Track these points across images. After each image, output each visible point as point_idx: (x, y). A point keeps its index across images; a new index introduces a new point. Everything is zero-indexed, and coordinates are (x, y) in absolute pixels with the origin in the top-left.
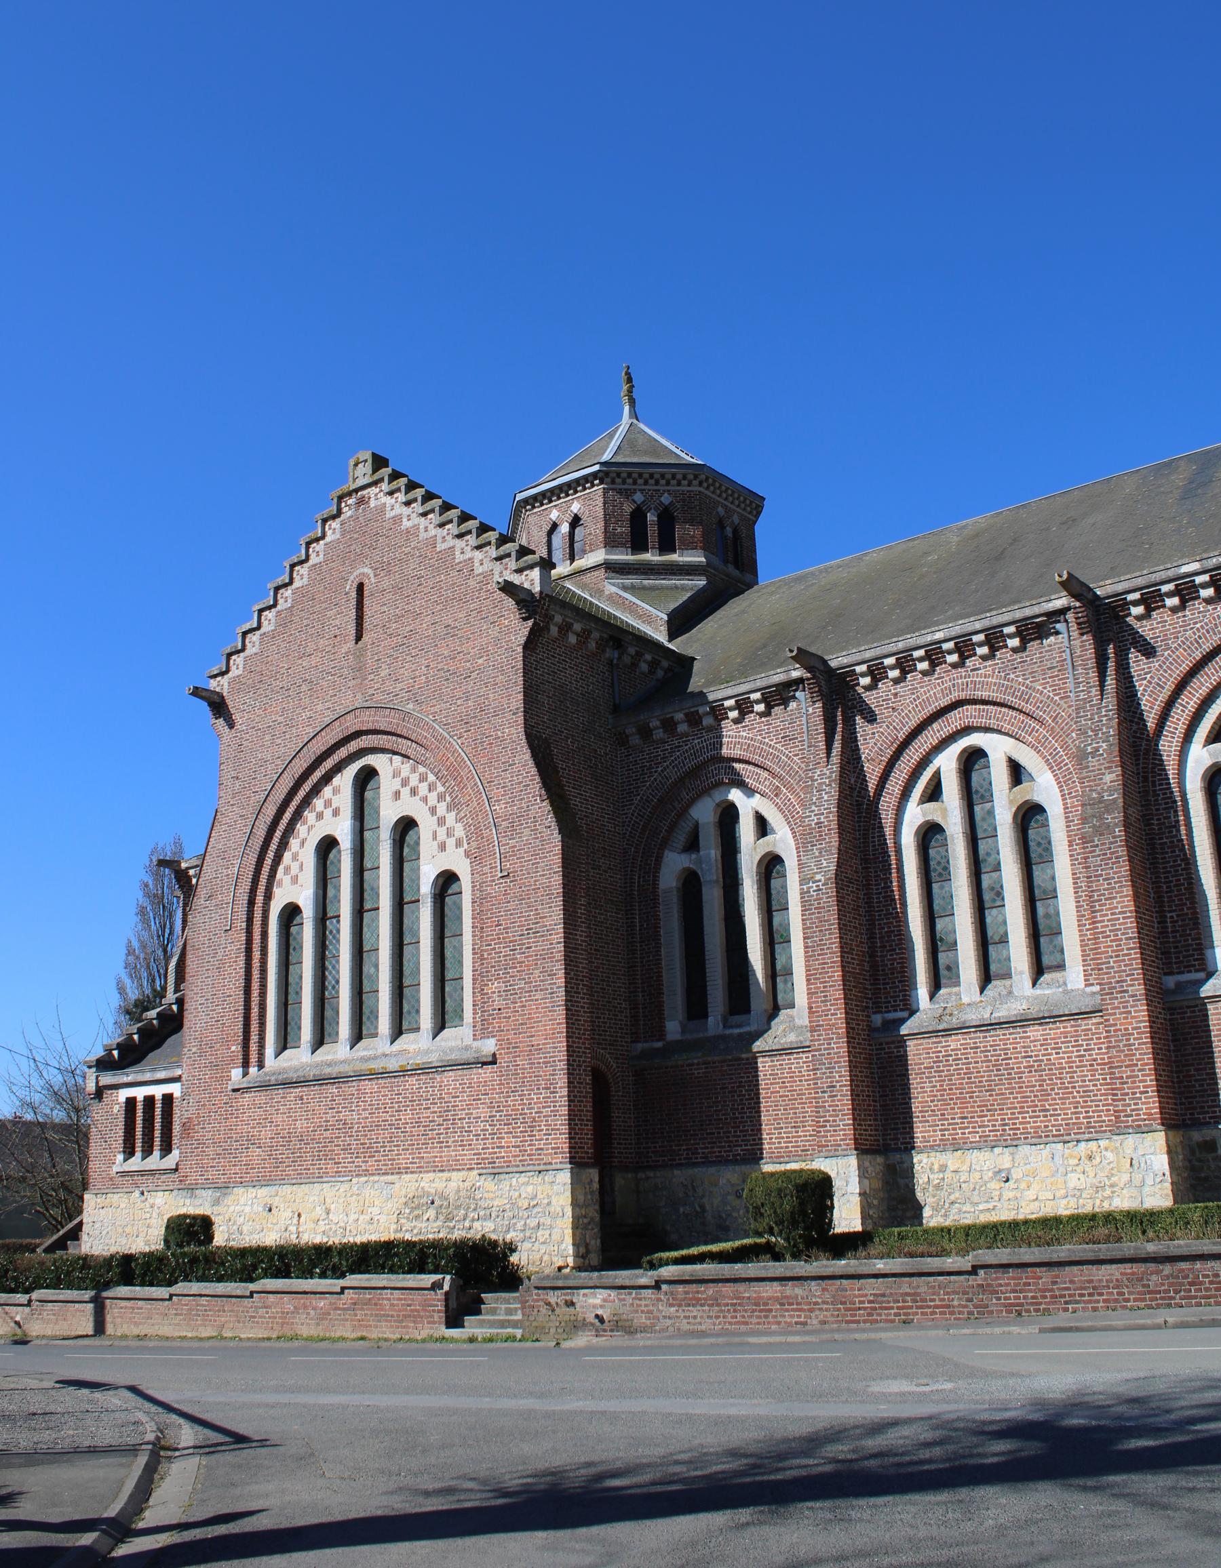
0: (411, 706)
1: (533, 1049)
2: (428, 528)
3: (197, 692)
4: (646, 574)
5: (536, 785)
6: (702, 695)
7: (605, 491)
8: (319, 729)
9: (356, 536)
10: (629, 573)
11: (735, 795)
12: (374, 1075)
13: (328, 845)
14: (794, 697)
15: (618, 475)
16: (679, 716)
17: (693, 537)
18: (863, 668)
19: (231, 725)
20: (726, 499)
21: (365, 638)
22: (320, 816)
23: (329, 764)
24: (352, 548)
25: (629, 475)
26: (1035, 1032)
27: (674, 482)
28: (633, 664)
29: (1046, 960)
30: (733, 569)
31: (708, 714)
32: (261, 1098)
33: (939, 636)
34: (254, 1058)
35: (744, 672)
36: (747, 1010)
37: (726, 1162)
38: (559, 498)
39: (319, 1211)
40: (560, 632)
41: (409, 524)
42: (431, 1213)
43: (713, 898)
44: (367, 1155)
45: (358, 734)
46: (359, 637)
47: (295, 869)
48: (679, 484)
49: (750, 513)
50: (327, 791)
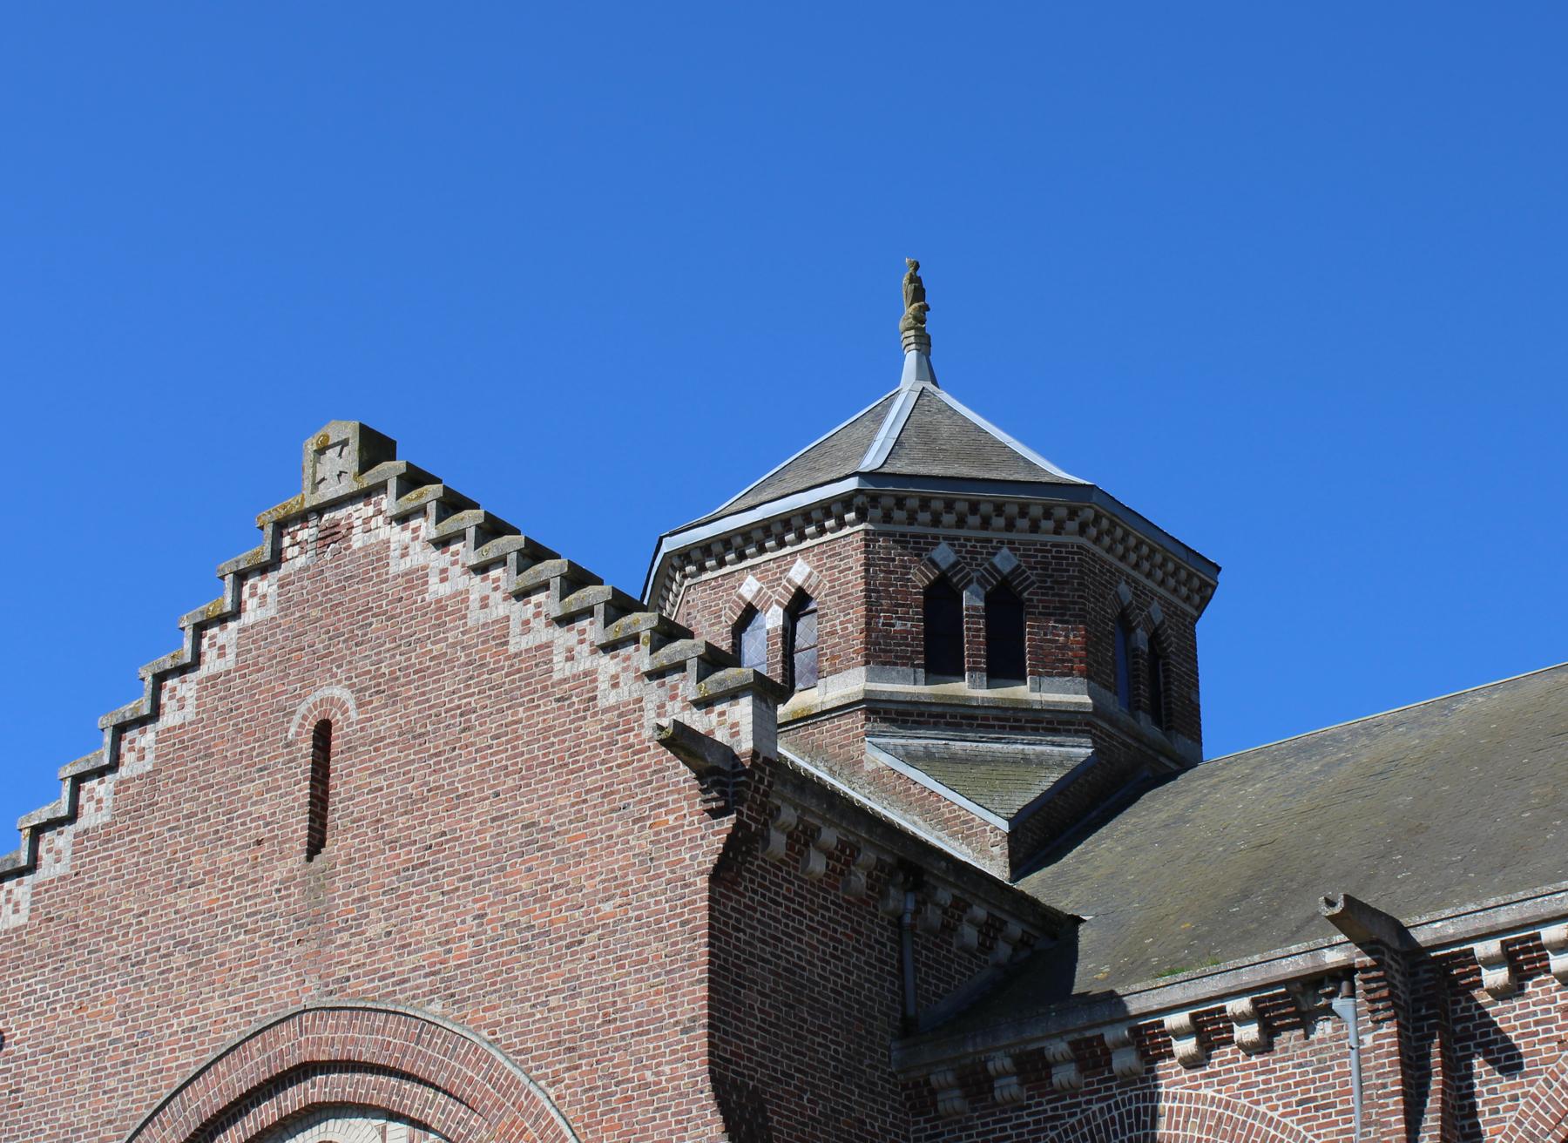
0: (437, 1007)
2: (489, 599)
4: (956, 726)
6: (1112, 1000)
7: (869, 539)
8: (210, 1056)
9: (316, 613)
10: (919, 724)
14: (1328, 1011)
15: (900, 502)
16: (1058, 1048)
17: (1064, 647)
18: (1492, 947)
20: (1136, 566)
21: (332, 848)
24: (306, 640)
25: (925, 503)
27: (1023, 523)
28: (945, 927)
30: (1148, 731)
31: (1125, 1044)
38: (762, 550)
40: (790, 847)
41: (444, 590)
46: (315, 846)
48: (1035, 528)
49: (1188, 599)
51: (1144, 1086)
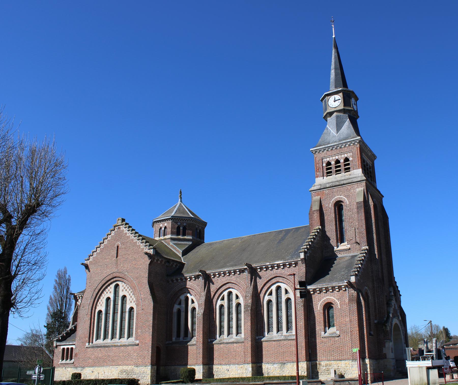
1: (145, 343)
2: (132, 236)
3: (82, 264)
5: (149, 292)
7: (172, 222)
11: (188, 295)
12: (115, 346)
13: (108, 299)
16: (179, 279)
19: (89, 271)
21: (118, 257)
22: (107, 293)
23: (109, 282)
26: (235, 345)
29: (239, 332)
30: (199, 238)
32: (92, 349)
33: (225, 270)
34: (91, 341)
35: (191, 272)
36: (187, 337)
37: (181, 365)
39: (103, 372)
42: (125, 373)
43: (183, 314)
44: (113, 362)
45: (116, 277)
46: (117, 257)
47: (101, 302)
50: (109, 288)
51: (186, 282)
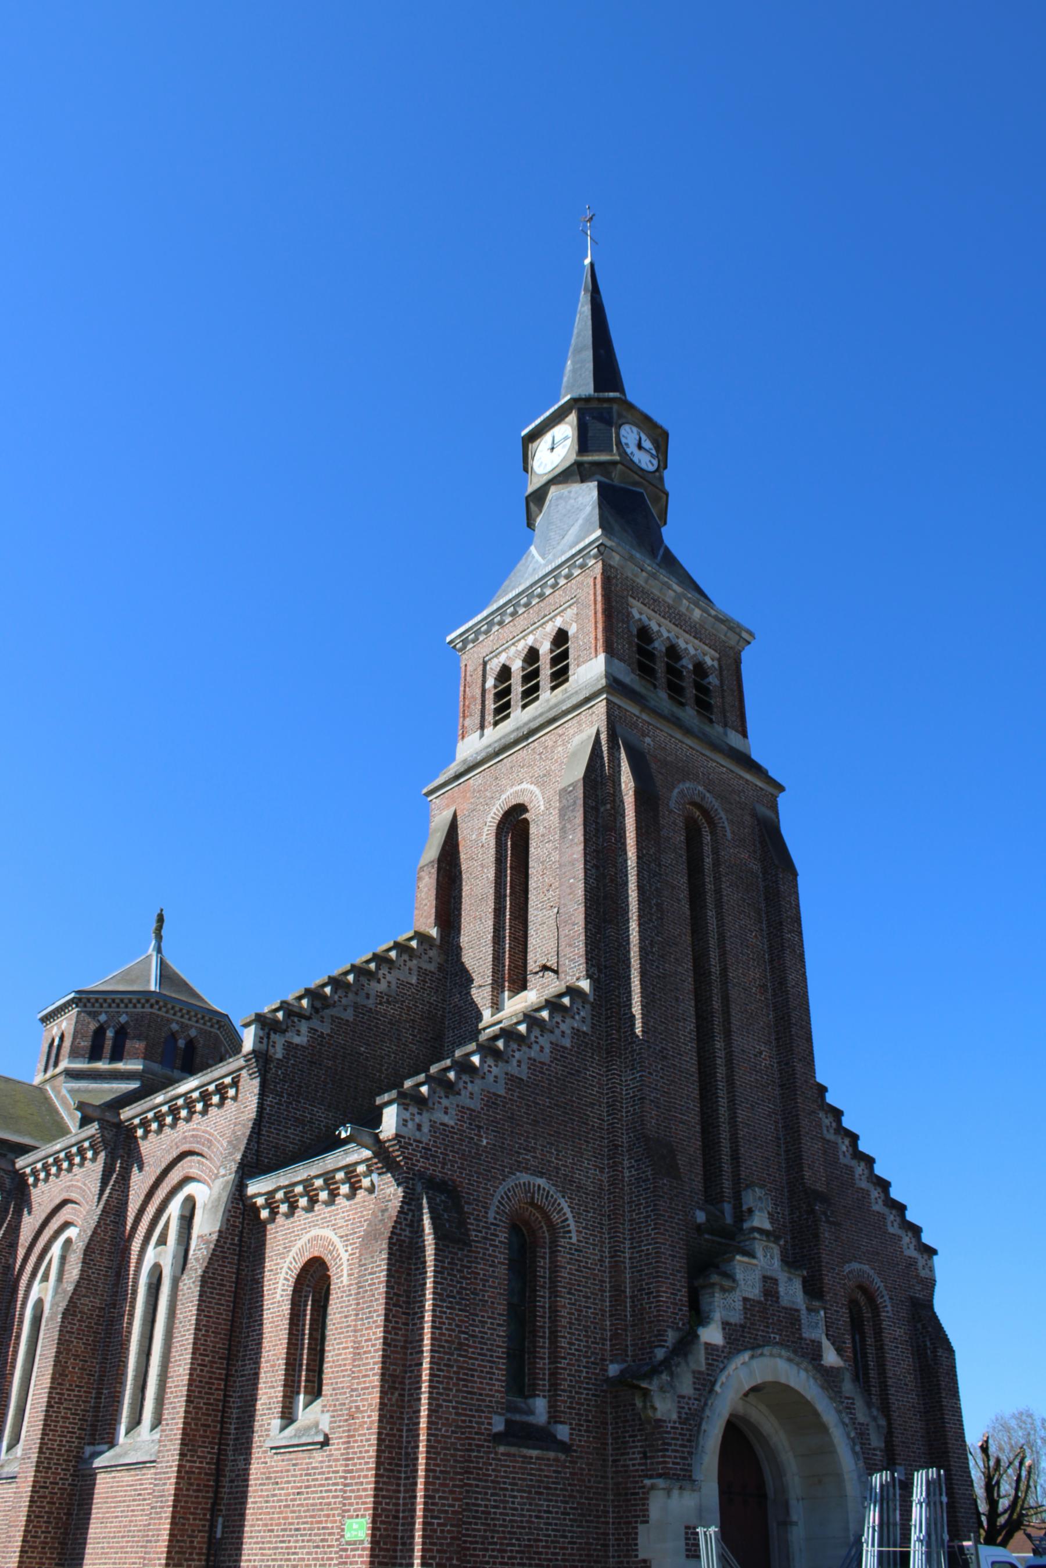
7: (79, 1013)
